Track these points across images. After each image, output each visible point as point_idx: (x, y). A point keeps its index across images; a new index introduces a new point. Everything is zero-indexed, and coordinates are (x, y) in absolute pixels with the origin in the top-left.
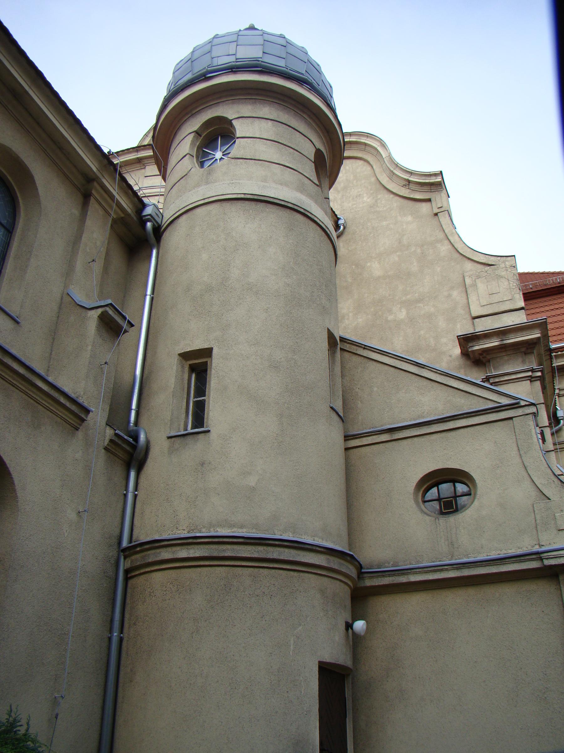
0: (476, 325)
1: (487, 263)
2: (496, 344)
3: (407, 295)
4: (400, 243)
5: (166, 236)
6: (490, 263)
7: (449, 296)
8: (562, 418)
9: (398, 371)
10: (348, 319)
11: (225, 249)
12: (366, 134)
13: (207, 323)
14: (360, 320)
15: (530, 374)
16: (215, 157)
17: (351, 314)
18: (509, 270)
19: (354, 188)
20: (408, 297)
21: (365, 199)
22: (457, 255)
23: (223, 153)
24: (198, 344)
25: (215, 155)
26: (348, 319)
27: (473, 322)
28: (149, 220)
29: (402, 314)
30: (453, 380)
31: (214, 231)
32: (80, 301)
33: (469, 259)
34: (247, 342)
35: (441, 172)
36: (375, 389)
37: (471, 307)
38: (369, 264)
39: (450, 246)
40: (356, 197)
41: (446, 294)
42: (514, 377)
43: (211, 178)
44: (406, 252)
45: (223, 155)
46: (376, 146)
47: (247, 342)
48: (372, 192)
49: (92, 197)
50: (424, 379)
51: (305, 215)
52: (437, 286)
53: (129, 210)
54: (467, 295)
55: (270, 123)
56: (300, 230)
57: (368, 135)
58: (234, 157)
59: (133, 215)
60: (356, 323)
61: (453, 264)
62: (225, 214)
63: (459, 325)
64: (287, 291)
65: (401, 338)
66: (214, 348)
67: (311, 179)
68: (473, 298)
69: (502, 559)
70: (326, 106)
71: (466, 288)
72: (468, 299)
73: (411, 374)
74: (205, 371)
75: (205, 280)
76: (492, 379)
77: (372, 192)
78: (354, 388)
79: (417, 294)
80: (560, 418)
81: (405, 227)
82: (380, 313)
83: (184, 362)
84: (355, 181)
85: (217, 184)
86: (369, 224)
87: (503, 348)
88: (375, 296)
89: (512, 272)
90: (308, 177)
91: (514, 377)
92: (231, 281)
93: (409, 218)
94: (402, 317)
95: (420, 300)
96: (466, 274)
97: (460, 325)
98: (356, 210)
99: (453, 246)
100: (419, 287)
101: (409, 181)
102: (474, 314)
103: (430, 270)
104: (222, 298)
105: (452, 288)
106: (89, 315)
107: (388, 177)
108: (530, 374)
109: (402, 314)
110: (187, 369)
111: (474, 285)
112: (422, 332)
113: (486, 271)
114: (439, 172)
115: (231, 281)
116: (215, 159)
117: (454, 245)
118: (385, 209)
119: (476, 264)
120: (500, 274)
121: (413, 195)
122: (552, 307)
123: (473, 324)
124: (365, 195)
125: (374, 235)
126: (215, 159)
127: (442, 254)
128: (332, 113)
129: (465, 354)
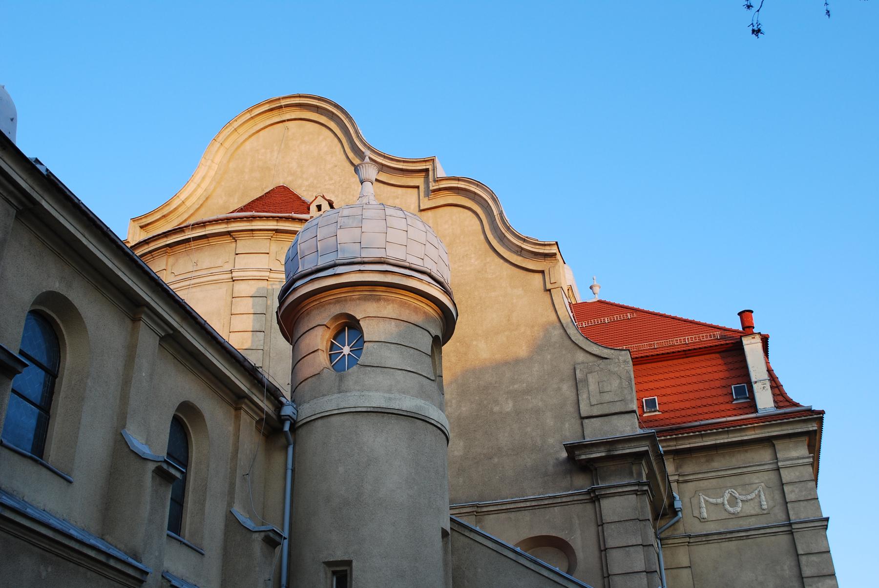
0: (584, 426)
1: (599, 355)
2: (603, 454)
3: (514, 384)
4: (509, 320)
5: (302, 432)
6: (602, 356)
7: (559, 389)
8: (680, 509)
9: (499, 555)
10: (451, 406)
11: (358, 464)
12: (477, 183)
13: (346, 536)
14: (464, 409)
15: (636, 488)
16: (342, 352)
17: (454, 401)
18: (622, 366)
19: (460, 246)
20: (516, 386)
21: (473, 261)
22: (568, 342)
23: (350, 348)
24: (339, 556)
25: (342, 352)
26: (451, 406)
27: (582, 423)
28: (288, 420)
29: (509, 406)
30: (545, 569)
31: (348, 444)
32: (244, 523)
33: (581, 348)
34: (379, 555)
35: (557, 243)
36: (480, 570)
37: (581, 406)
38: (475, 343)
39: (562, 331)
40: (463, 257)
41: (555, 386)
42: (620, 490)
43: (343, 385)
44: (515, 333)
45: (351, 351)
46: (487, 199)
47: (379, 555)
48: (480, 252)
49: (242, 410)
50: (521, 566)
51: (425, 421)
52: (546, 377)
53: (270, 412)
54: (577, 391)
55: (393, 322)
56: (420, 437)
57: (479, 184)
58: (362, 364)
59: (274, 417)
60: (459, 411)
61: (564, 352)
62: (357, 426)
63: (567, 424)
64: (410, 503)
65: (506, 435)
66: (353, 561)
67: (429, 376)
68: (583, 397)
69: (726, 470)
70: (443, 294)
71: (576, 383)
72: (578, 395)
73: (510, 560)
74: (346, 576)
75: (343, 494)
76: (599, 491)
77: (480, 252)
78: (462, 567)
79: (525, 384)
80: (677, 510)
81: (515, 301)
82: (485, 402)
83: (327, 569)
84: (462, 237)
85: (349, 394)
86: (476, 293)
87: (609, 458)
88: (480, 382)
89: (626, 368)
90: (426, 376)
91: (620, 490)
92: (365, 497)
93: (520, 291)
94: (508, 410)
95: (528, 391)
96: (577, 367)
97: (569, 424)
98: (462, 274)
99: (565, 331)
100: (528, 376)
101: (522, 249)
102: (583, 414)
103: (539, 357)
104: (358, 513)
105: (562, 380)
106: (253, 537)
107: (499, 237)
108: (636, 488)
109: (509, 406)
110: (329, 574)
111: (585, 381)
112: (529, 429)
113: (599, 365)
114: (555, 243)
115: (365, 497)
116: (343, 354)
117: (567, 331)
118: (494, 276)
119: (588, 356)
120: (613, 370)
121: (525, 264)
122: (677, 374)
123: (582, 424)
124: (473, 256)
125: (481, 307)
126: (343, 354)
127: (553, 340)
128: (448, 297)
129: (571, 458)
